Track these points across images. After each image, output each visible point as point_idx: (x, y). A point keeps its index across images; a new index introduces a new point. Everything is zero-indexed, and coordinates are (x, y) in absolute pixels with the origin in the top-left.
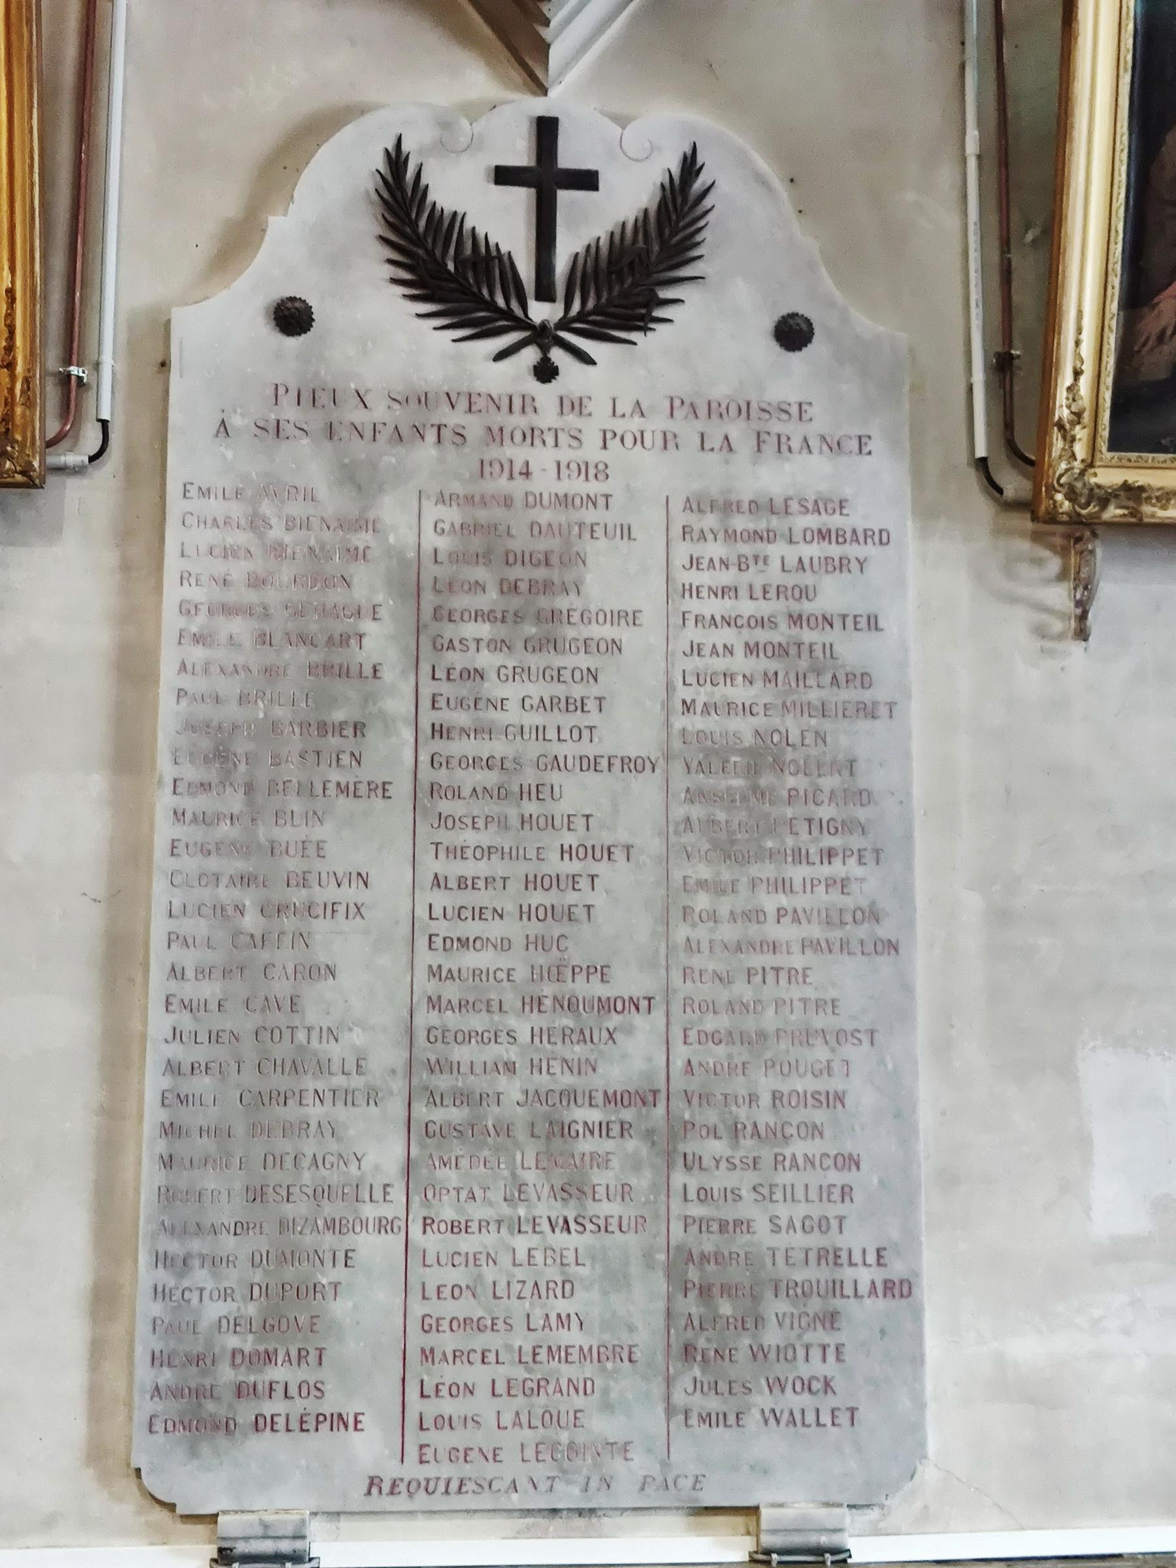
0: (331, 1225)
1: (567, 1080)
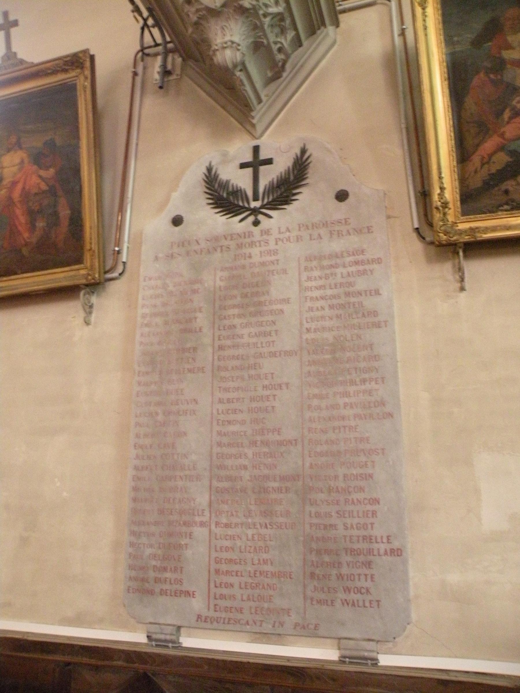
0: (185, 524)
1: (266, 472)
